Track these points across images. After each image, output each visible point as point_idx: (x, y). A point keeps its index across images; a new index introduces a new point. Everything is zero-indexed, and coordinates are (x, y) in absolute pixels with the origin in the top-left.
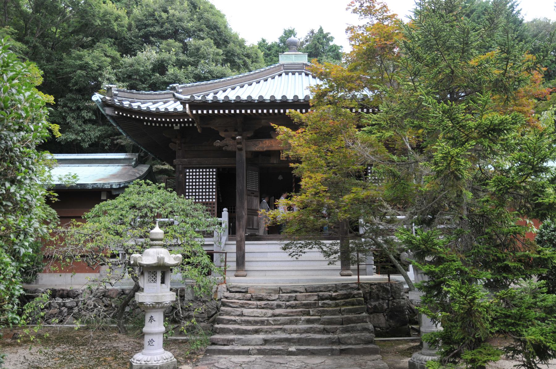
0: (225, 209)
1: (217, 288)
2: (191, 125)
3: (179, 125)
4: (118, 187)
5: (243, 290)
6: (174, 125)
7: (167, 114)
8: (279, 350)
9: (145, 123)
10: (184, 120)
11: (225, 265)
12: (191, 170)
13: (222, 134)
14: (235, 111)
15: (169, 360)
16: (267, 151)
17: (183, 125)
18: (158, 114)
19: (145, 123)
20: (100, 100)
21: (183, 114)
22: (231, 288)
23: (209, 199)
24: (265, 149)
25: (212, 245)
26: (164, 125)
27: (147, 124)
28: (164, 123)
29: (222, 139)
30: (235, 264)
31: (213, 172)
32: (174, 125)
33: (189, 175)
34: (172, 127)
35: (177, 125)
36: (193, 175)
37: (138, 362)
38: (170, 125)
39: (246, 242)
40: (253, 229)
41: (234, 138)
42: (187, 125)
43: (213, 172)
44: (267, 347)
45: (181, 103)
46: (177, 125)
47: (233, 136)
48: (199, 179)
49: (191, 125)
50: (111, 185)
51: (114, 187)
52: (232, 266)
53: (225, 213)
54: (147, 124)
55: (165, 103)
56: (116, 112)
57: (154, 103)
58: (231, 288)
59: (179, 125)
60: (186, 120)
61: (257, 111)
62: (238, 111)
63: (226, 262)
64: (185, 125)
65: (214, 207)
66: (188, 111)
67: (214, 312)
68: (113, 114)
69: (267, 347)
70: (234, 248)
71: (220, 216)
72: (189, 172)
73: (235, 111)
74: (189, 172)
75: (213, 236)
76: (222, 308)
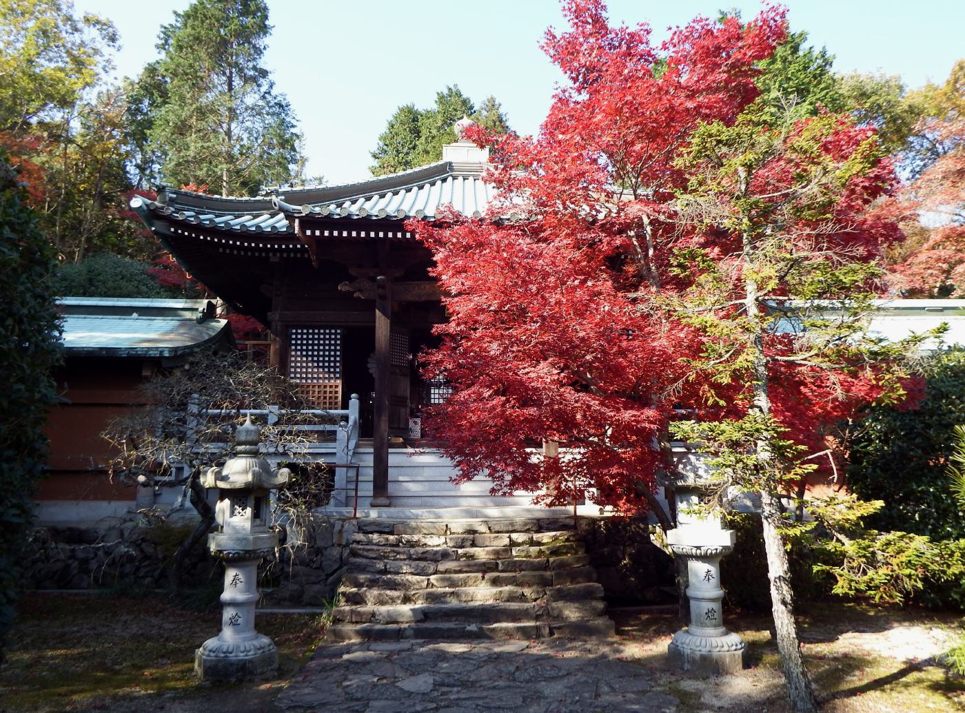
0: (353, 395)
1: (343, 526)
2: (299, 255)
3: (278, 254)
4: (173, 354)
5: (387, 530)
6: (271, 254)
7: (259, 235)
8: (450, 630)
9: (221, 250)
10: (287, 246)
11: (356, 490)
12: (322, 331)
13: (353, 272)
14: (377, 234)
15: (266, 649)
16: (427, 302)
17: (285, 255)
18: (245, 234)
19: (221, 250)
20: (145, 208)
21: (289, 236)
22: (365, 525)
23: (307, 378)
24: (423, 299)
25: (334, 454)
26: (260, 254)
27: (224, 251)
28: (246, 249)
29: (352, 279)
30: (371, 486)
31: (336, 334)
32: (271, 254)
33: (296, 339)
34: (267, 257)
35: (275, 255)
36: (319, 339)
37: (212, 654)
38: (264, 254)
39: (390, 450)
40: (399, 428)
41: (373, 279)
42: (292, 255)
43: (336, 334)
44: (429, 625)
45: (287, 217)
46: (275, 255)
47: (371, 274)
48: (313, 345)
49: (299, 255)
50: (161, 352)
51: (166, 354)
52: (367, 489)
53: (354, 402)
54: (224, 251)
55: (255, 217)
56: (172, 230)
57: (236, 217)
58: (365, 525)
59: (278, 254)
60: (299, 246)
61: (358, 234)
62: (363, 234)
63: (357, 481)
64: (289, 255)
65: (336, 392)
66: (297, 230)
67: (336, 567)
68: (166, 232)
69: (429, 625)
70: (369, 460)
71: (345, 406)
72: (297, 334)
73: (349, 234)
74: (297, 334)
75: (335, 440)
76: (353, 560)
